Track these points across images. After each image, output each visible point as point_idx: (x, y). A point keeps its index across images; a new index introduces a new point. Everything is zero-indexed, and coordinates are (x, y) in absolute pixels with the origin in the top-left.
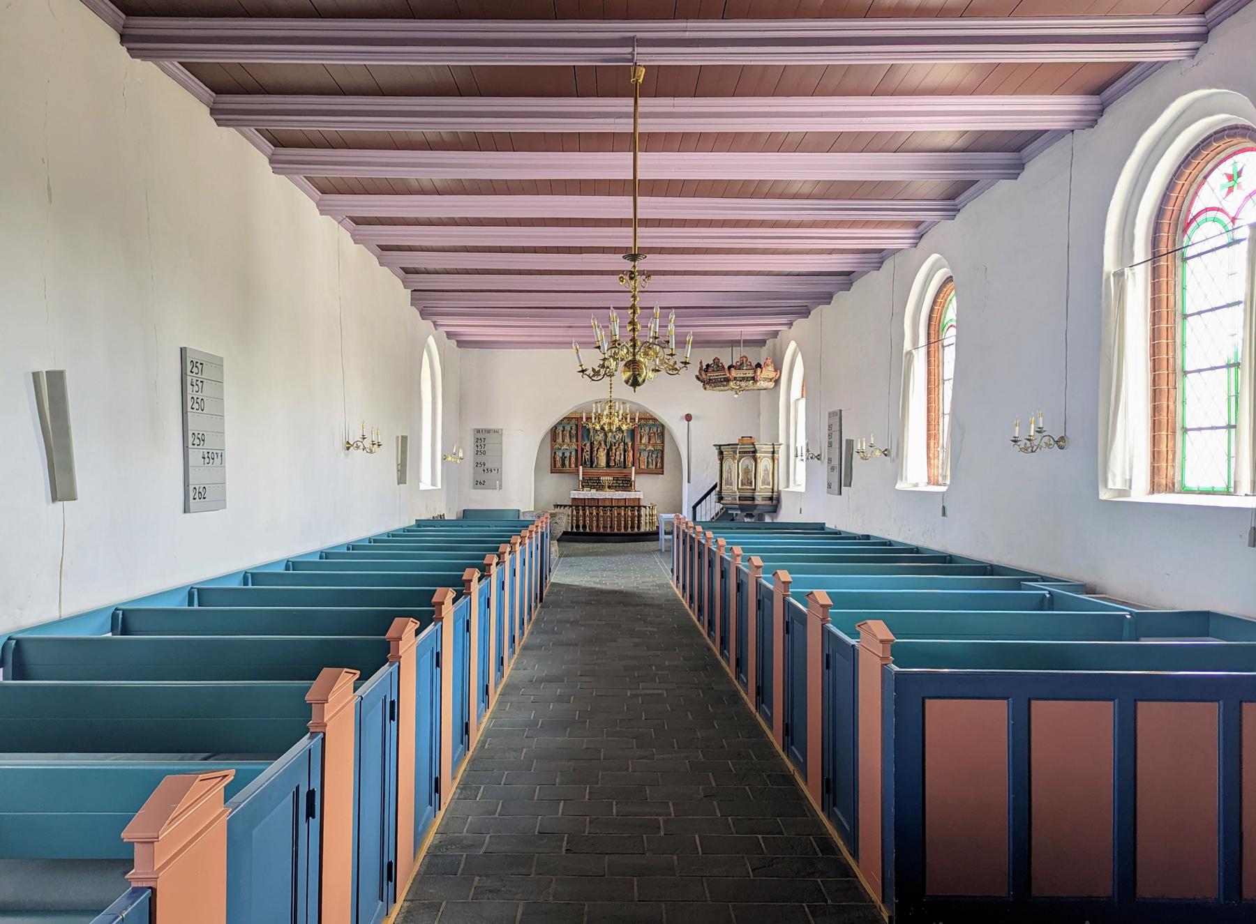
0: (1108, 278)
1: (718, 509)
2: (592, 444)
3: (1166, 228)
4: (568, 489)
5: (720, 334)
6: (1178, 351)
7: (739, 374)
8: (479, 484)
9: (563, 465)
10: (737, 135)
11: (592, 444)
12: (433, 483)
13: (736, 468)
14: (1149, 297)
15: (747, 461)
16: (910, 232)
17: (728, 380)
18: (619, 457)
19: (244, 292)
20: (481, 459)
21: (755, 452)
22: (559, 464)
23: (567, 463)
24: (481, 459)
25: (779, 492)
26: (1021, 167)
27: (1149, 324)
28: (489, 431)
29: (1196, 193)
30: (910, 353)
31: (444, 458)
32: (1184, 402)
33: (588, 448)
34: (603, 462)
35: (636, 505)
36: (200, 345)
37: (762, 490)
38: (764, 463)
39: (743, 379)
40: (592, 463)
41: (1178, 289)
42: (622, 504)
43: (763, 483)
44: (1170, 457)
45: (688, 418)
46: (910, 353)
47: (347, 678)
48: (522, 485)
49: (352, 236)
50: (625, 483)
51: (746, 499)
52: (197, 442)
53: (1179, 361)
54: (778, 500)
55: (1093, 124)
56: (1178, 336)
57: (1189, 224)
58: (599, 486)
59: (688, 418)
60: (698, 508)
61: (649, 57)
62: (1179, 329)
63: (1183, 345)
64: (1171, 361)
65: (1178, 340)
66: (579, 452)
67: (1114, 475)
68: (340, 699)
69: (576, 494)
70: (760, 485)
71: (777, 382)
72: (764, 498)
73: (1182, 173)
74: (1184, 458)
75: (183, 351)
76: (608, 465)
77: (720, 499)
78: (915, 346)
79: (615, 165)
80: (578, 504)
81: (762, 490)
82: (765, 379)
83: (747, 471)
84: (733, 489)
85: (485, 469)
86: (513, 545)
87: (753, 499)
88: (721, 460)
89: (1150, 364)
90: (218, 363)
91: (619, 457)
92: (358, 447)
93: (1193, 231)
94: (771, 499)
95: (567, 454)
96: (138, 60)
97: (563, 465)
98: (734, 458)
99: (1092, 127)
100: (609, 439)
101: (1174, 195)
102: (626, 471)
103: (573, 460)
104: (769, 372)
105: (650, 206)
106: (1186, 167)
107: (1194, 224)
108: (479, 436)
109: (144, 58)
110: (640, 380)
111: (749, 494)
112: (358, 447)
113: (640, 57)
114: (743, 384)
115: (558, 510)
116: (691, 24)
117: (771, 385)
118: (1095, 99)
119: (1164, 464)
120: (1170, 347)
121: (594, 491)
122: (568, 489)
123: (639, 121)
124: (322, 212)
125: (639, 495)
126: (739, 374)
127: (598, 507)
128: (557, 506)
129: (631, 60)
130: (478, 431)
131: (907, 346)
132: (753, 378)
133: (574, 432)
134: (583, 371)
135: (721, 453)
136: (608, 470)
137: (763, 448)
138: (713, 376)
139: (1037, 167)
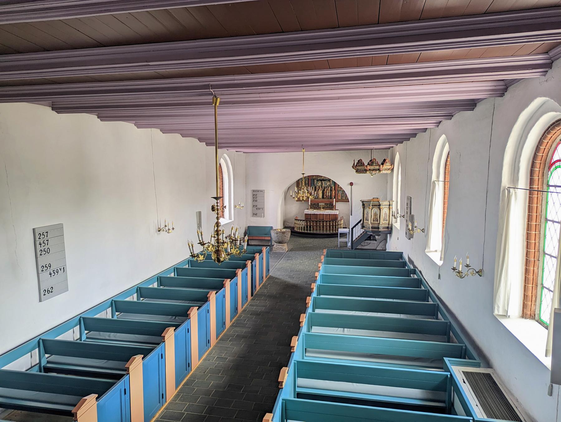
0: (504, 190)
1: (362, 232)
2: (315, 187)
3: (538, 166)
6: (542, 239)
7: (372, 168)
8: (255, 215)
11: (315, 187)
12: (230, 218)
13: (371, 212)
14: (527, 204)
15: (376, 210)
17: (366, 171)
18: (328, 193)
20: (255, 203)
21: (380, 205)
24: (255, 203)
25: (392, 224)
27: (526, 220)
29: (556, 148)
30: (434, 182)
31: (235, 207)
32: (543, 269)
34: (321, 196)
35: (334, 218)
36: (41, 223)
37: (383, 224)
38: (385, 211)
39: (374, 170)
41: (544, 202)
43: (384, 220)
44: (534, 299)
46: (434, 182)
47: (172, 329)
51: (375, 228)
53: (541, 245)
54: (392, 228)
55: (502, 95)
56: (542, 230)
57: (551, 165)
59: (351, 184)
62: (543, 226)
63: (545, 236)
64: (537, 244)
65: (542, 233)
67: (498, 307)
68: (228, 283)
71: (393, 170)
72: (384, 228)
73: (546, 137)
74: (541, 301)
75: (34, 230)
76: (323, 197)
77: (363, 227)
78: (438, 177)
80: (308, 217)
81: (383, 224)
82: (386, 169)
83: (375, 214)
84: (369, 223)
85: (257, 208)
87: (378, 228)
88: (364, 208)
89: (525, 243)
90: (60, 227)
92: (163, 230)
93: (553, 171)
94: (388, 228)
98: (369, 208)
99: (502, 96)
100: (323, 185)
101: (546, 141)
102: (331, 200)
104: (387, 166)
106: (548, 134)
107: (554, 167)
108: (255, 193)
111: (376, 226)
112: (163, 230)
115: (297, 222)
117: (389, 172)
119: (530, 303)
120: (537, 236)
122: (297, 210)
123: (218, 118)
124: (138, 127)
125: (336, 212)
126: (372, 168)
130: (254, 191)
131: (434, 178)
132: (379, 170)
133: (307, 182)
135: (363, 205)
137: (384, 204)
138: (359, 167)
139: (479, 108)
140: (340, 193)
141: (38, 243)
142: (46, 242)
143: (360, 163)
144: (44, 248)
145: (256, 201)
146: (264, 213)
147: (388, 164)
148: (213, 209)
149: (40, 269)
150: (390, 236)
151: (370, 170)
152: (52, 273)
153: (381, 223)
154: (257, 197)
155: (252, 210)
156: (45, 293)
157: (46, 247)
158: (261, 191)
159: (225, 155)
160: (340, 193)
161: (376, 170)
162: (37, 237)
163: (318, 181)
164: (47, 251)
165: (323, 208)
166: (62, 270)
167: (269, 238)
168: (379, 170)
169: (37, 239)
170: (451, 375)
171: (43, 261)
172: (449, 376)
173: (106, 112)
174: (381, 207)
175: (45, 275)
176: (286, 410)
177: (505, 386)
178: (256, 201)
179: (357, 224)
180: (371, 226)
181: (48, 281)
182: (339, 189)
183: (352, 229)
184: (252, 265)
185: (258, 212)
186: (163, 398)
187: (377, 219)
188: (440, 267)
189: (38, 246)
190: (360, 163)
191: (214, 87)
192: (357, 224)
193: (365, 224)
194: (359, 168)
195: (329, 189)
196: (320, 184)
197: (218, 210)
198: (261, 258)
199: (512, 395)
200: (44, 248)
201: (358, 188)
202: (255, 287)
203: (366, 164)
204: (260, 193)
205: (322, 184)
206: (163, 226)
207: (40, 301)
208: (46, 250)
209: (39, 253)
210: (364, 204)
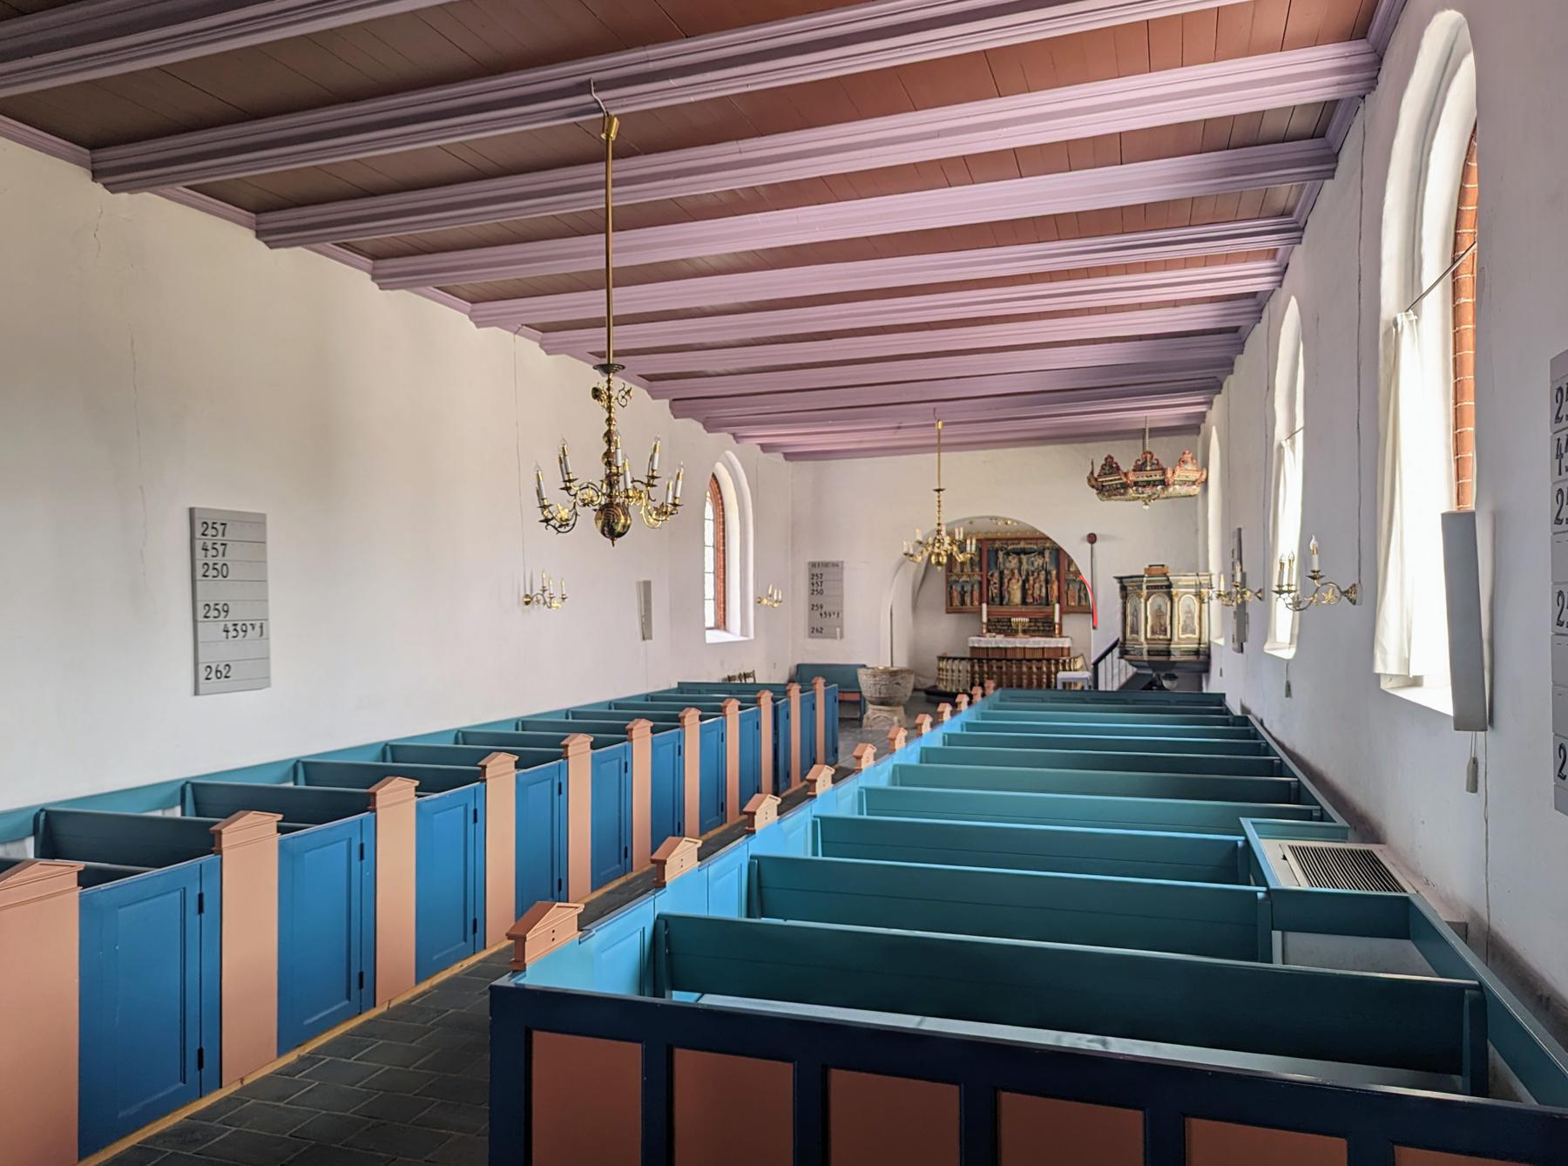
2: (1001, 573)
4: (946, 634)
5: (1117, 422)
7: (1143, 478)
8: (816, 631)
9: (963, 602)
10: (940, 163)
11: (1001, 573)
12: (744, 632)
13: (1147, 607)
15: (1158, 600)
16: (1265, 266)
17: (1125, 486)
18: (1038, 590)
19: (320, 438)
20: (818, 600)
21: (1170, 586)
22: (957, 602)
23: (968, 600)
24: (818, 600)
26: (1335, 158)
27: (1452, 401)
28: (826, 565)
31: (758, 601)
33: (996, 579)
34: (1017, 597)
36: (213, 501)
38: (1185, 602)
40: (1002, 598)
42: (1019, 656)
43: (1184, 631)
45: (1092, 539)
48: (881, 628)
49: (541, 346)
50: (1046, 627)
51: (1158, 653)
52: (213, 613)
58: (1010, 631)
59: (1092, 539)
60: (1101, 665)
61: (623, 104)
66: (984, 584)
67: (1385, 652)
69: (975, 641)
70: (1178, 634)
72: (1188, 652)
75: (192, 510)
76: (1024, 602)
77: (1124, 653)
79: (584, 254)
82: (1184, 483)
83: (1159, 614)
84: (1143, 638)
85: (823, 612)
86: (955, 705)
87: (1168, 653)
90: (259, 521)
91: (1038, 590)
94: (1197, 653)
95: (968, 588)
96: (125, 195)
97: (963, 602)
100: (1025, 566)
102: (1047, 609)
103: (976, 594)
105: (629, 299)
109: (132, 187)
110: (619, 528)
111: (1162, 647)
113: (609, 104)
114: (1148, 491)
115: (943, 664)
116: (652, 52)
118: (1359, 46)
121: (1000, 637)
122: (946, 634)
124: (479, 325)
125: (1066, 643)
127: (980, 660)
128: (941, 658)
129: (600, 110)
130: (814, 565)
132: (1164, 483)
134: (547, 521)
135: (1123, 588)
136: (1024, 609)
137: (1183, 584)
138: (1108, 482)
140: (1074, 587)
141: (199, 545)
142: (221, 549)
143: (1110, 467)
144: (215, 560)
145: (821, 592)
146: (841, 627)
147: (1189, 467)
148: (596, 393)
149: (201, 612)
150: (1208, 679)
151: (1136, 484)
152: (231, 628)
153: (1175, 639)
154: (822, 580)
155: (810, 618)
156: (210, 675)
157: (220, 560)
158: (835, 565)
159: (730, 454)
160: (1074, 587)
161: (1154, 484)
162: (199, 529)
163: (1008, 554)
164: (222, 572)
165: (1024, 632)
166: (257, 628)
167: (856, 697)
168: (1164, 483)
169: (198, 535)
170: (1247, 841)
171: (211, 591)
172: (1240, 844)
173: (391, 262)
174: (1174, 591)
175: (211, 630)
176: (760, 887)
177: (1407, 867)
178: (821, 592)
179: (1110, 650)
180: (1145, 646)
181: (218, 650)
182: (1071, 576)
183: (1096, 664)
184: (775, 710)
185: (826, 622)
186: (475, 931)
188: (1288, 661)
189: (199, 553)
190: (1110, 467)
191: (602, 86)
192: (1110, 650)
193: (1129, 645)
194: (1108, 480)
195: (1042, 577)
196: (1013, 562)
197: (610, 397)
198: (808, 705)
199: (1415, 874)
200: (215, 560)
201: (1109, 541)
202: (788, 775)
203: (1124, 469)
204: (830, 569)
205: (1020, 562)
206: (537, 590)
207: (196, 693)
208: (210, 532)
209: (200, 571)
210: (1127, 587)
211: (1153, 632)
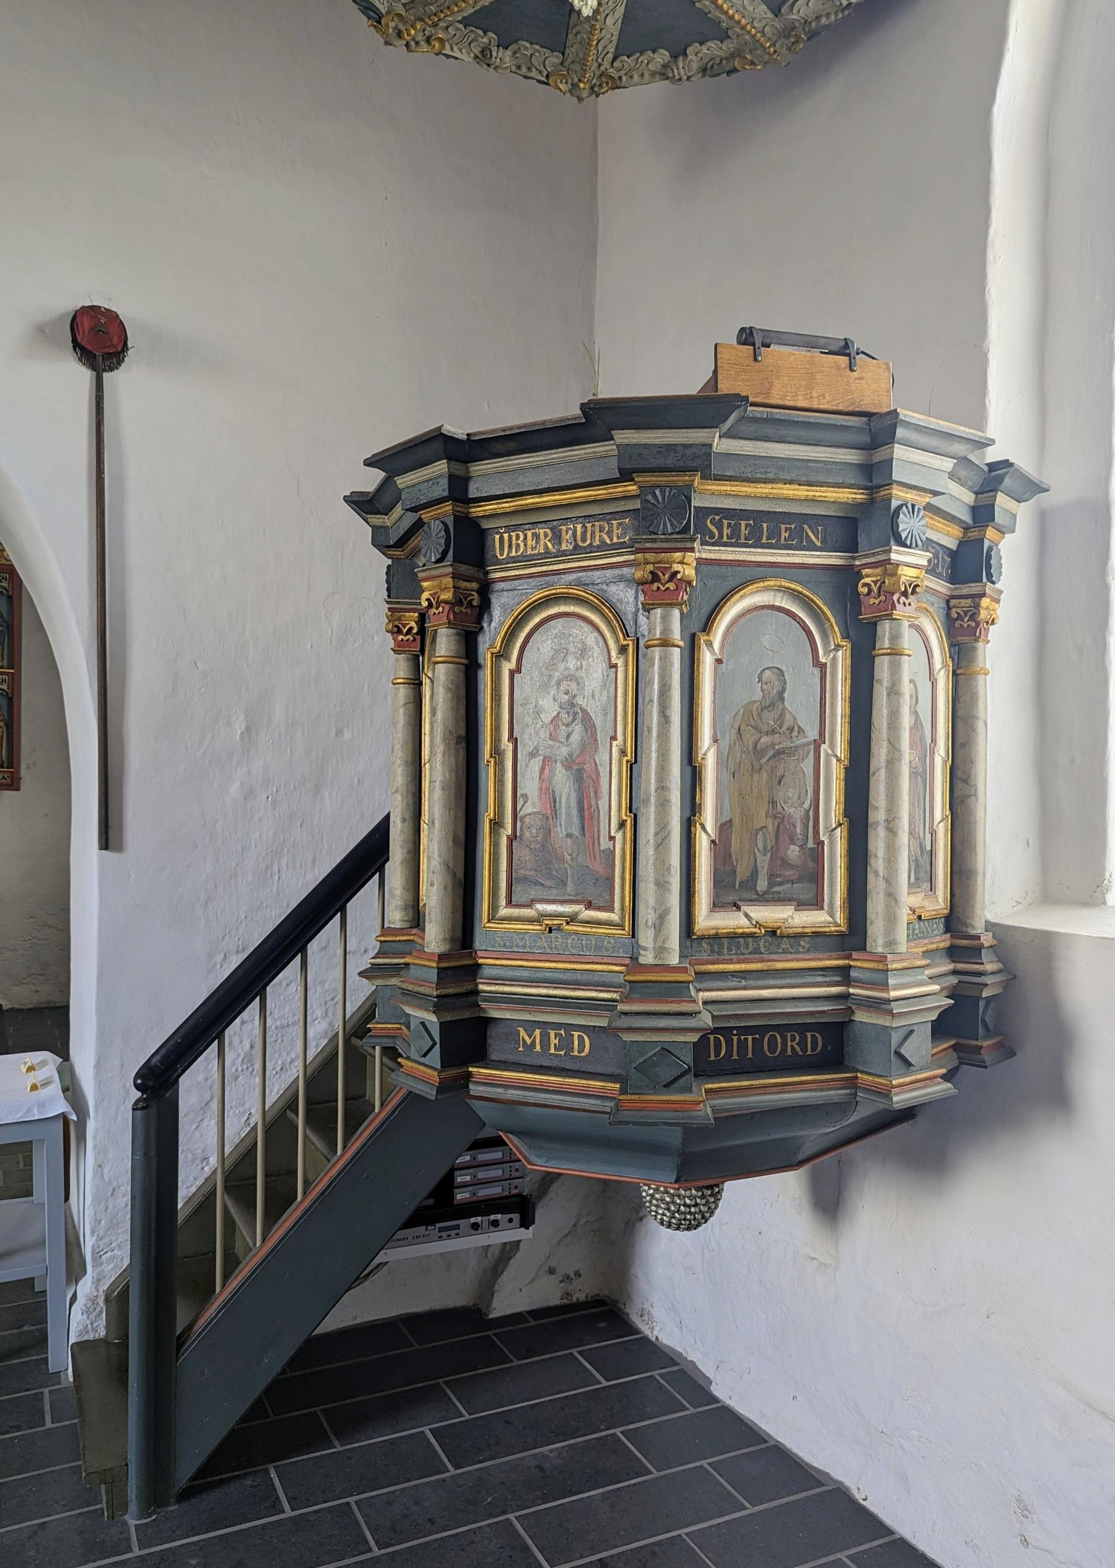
45: (98, 340)
60: (195, 1085)
83: (765, 742)
111: (800, 993)
187: (810, 827)
210: (443, 527)
211: (731, 889)
